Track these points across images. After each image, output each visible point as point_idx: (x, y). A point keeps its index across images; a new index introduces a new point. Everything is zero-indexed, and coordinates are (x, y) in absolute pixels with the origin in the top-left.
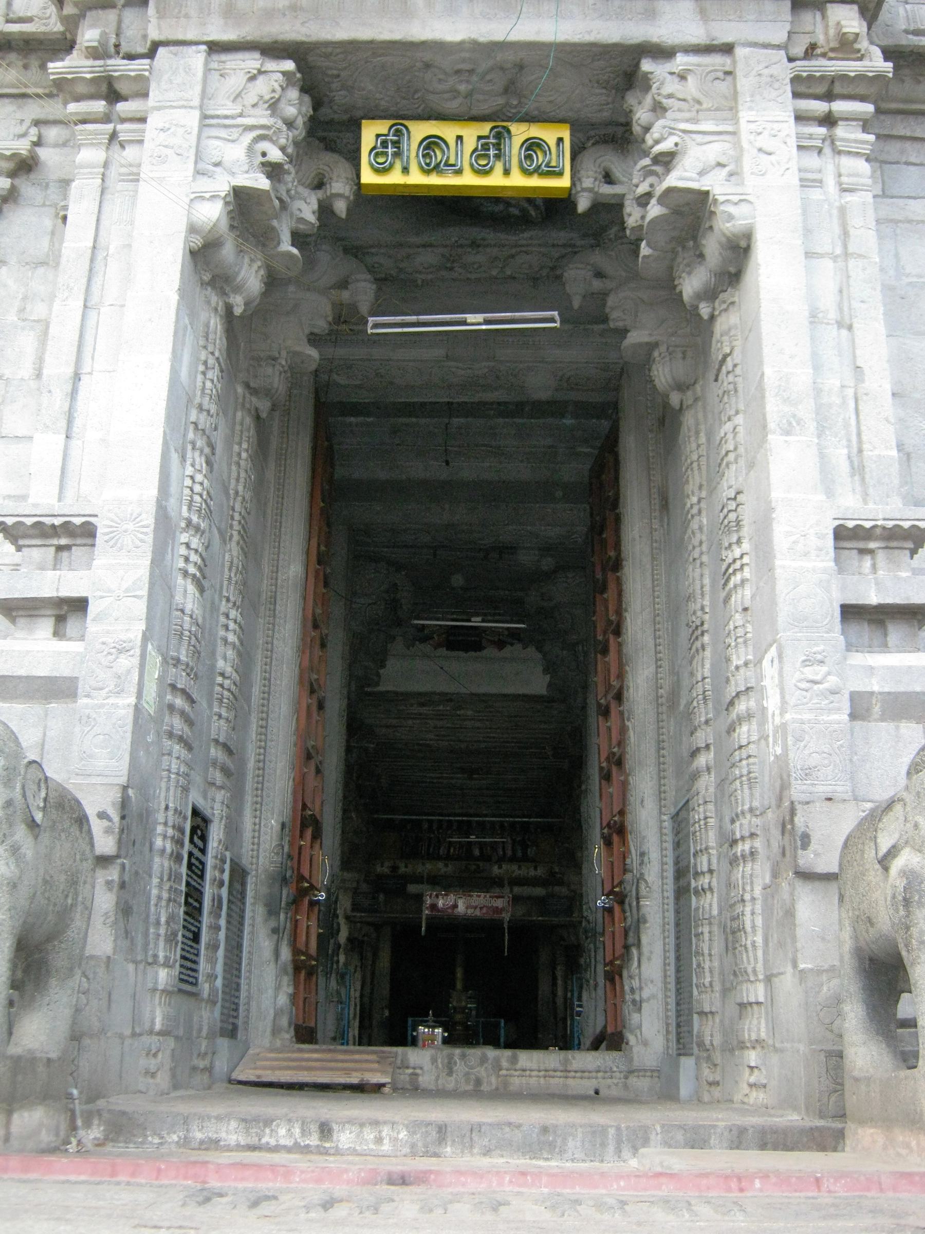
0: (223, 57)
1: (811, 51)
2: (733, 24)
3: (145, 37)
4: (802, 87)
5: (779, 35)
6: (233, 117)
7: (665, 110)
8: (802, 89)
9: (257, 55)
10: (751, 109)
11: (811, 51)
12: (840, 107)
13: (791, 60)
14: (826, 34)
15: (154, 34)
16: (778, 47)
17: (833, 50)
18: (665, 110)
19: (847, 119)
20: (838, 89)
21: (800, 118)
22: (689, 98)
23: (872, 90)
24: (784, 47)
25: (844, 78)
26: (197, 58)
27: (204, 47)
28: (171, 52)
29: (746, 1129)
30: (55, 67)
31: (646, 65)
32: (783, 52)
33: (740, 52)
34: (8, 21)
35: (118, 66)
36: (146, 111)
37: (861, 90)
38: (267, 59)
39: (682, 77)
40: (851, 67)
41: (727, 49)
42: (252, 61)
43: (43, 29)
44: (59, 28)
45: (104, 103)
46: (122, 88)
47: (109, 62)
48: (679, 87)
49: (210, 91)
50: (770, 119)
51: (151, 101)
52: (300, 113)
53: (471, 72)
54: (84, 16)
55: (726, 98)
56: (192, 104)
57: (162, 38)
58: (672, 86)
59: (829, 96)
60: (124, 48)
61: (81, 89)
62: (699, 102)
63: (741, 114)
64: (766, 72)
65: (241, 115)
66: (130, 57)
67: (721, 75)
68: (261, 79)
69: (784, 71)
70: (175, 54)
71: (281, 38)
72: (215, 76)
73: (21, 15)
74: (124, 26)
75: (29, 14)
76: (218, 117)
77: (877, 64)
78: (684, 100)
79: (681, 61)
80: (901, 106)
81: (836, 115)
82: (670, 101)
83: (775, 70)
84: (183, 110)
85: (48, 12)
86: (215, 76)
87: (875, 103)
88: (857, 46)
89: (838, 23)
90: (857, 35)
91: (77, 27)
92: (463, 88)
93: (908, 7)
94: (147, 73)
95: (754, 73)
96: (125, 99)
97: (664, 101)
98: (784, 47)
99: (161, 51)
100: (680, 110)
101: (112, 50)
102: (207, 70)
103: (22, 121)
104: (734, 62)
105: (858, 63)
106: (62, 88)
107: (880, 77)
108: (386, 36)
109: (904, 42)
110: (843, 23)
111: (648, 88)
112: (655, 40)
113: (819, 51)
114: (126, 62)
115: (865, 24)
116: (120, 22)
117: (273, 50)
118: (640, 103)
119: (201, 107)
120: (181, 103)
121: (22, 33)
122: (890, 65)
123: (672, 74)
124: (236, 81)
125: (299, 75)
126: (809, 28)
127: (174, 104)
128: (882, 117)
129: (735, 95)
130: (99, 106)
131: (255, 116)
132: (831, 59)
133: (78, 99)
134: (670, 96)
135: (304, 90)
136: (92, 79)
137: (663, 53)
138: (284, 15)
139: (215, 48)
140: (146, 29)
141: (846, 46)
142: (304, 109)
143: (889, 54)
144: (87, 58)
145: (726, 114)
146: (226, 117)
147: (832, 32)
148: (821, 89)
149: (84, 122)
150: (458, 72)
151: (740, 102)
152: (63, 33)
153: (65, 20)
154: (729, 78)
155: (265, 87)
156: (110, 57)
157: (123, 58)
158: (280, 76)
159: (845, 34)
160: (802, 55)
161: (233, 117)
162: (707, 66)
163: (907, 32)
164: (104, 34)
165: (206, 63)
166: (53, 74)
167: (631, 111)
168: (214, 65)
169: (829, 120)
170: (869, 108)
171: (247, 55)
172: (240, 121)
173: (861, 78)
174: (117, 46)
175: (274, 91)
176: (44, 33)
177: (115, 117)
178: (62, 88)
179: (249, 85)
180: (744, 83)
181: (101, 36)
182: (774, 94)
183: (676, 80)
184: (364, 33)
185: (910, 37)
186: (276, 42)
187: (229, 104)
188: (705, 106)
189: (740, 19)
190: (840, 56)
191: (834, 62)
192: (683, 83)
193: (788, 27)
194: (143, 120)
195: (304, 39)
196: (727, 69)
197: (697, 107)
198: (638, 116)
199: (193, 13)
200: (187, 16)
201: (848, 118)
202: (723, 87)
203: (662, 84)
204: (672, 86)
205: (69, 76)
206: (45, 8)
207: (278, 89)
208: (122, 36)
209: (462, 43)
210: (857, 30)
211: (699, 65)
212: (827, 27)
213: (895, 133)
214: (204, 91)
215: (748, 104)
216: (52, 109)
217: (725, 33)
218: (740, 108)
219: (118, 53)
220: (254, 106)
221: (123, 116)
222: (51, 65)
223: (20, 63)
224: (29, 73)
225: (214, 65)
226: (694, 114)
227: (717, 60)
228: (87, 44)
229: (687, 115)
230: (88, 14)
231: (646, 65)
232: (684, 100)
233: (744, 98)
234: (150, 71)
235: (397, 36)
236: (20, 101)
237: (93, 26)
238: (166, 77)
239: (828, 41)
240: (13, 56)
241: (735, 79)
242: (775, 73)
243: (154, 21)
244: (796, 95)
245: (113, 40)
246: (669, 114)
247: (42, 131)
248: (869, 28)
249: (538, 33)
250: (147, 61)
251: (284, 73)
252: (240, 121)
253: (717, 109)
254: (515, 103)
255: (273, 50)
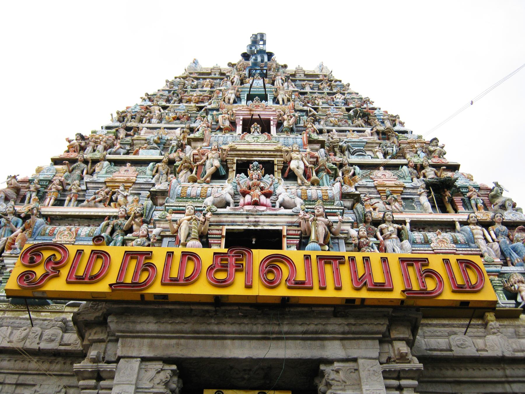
0: (147, 363)
1: (389, 360)
2: (356, 350)
3: (116, 354)
4: (387, 375)
5: (376, 354)
6: (149, 389)
7: (331, 385)
8: (387, 375)
9: (161, 363)
10: (367, 384)
11: (389, 360)
12: (404, 382)
13: (381, 363)
14: (394, 352)
15: (119, 354)
16: (375, 359)
17: (397, 359)
18: (331, 385)
19: (407, 387)
20: (402, 375)
21: (388, 388)
22: (341, 380)
23: (416, 375)
24: (378, 359)
25: (404, 371)
26: (136, 364)
27: (139, 359)
28: (126, 361)
29: (21, 202)
30: (76, 366)
31: (322, 367)
32: (377, 361)
33: (360, 361)
34: (60, 345)
35: (103, 366)
36: (112, 385)
37: (411, 375)
38: (165, 365)
39: (337, 371)
40: (406, 366)
41: (355, 360)
42: (159, 365)
43: (74, 348)
44: (81, 348)
45: (95, 381)
46: (103, 375)
47: (100, 364)
48: (337, 376)
49: (140, 377)
50: (375, 388)
51: (115, 381)
52: (178, 386)
53: (250, 370)
54: (92, 345)
55: (356, 380)
56: (132, 383)
57: (123, 355)
58: (333, 375)
59: (399, 378)
60: (107, 359)
61: (86, 375)
62: (345, 382)
63: (363, 387)
64: (371, 369)
65: (152, 388)
66: (108, 362)
67: (353, 371)
68: (162, 372)
69: (379, 368)
70: (127, 362)
71: (172, 356)
72: (143, 371)
73: (66, 342)
74: (107, 350)
75: (69, 342)
76: (142, 388)
77: (416, 364)
78: (339, 381)
79: (336, 365)
80: (430, 379)
81: (403, 386)
82: (333, 382)
83: (375, 368)
84: (128, 385)
85: (78, 342)
86: (143, 371)
87: (418, 380)
88: (407, 357)
89: (399, 349)
90: (407, 353)
91: (88, 349)
92: (246, 376)
93: (425, 340)
94: (114, 370)
95: (367, 369)
96: (104, 380)
97: (330, 382)
98: (378, 359)
99: (122, 360)
100: (337, 385)
101: (101, 359)
102: (140, 368)
103: (59, 386)
104: (358, 365)
105: (409, 364)
106: (80, 375)
107: (418, 370)
108: (215, 356)
109: (426, 354)
110: (400, 348)
111: (323, 376)
112: (325, 357)
113: (392, 360)
114: (106, 364)
115: (409, 348)
116: (106, 348)
117: (167, 361)
118: (320, 382)
119: (136, 384)
120: (127, 382)
121: (65, 350)
122: (422, 365)
123: (332, 370)
124: (152, 373)
125: (178, 371)
126: (387, 350)
127: (125, 383)
128: (422, 384)
129: (360, 378)
130: (93, 382)
131: (158, 388)
132: (397, 363)
133: (84, 379)
134: (333, 380)
135: (179, 377)
136: (91, 371)
137: (329, 362)
138: (173, 347)
139: (144, 359)
140: (116, 351)
141: (403, 358)
142: (179, 385)
143: (421, 359)
144: (90, 362)
145: (357, 387)
146: (146, 388)
147: (396, 352)
148: (395, 375)
149: (86, 389)
150: (245, 370)
151: (362, 382)
152: (82, 351)
153: (83, 346)
154: (357, 372)
155: (162, 376)
156: (100, 362)
157: (105, 363)
158: (170, 372)
159: (402, 353)
160: (385, 361)
161: (149, 389)
162: (347, 367)
163: (426, 350)
164: (99, 353)
165: (140, 366)
166: (76, 368)
167: (317, 386)
168: (143, 367)
169: (400, 388)
170: (416, 382)
171: (157, 363)
172: (152, 390)
173: (411, 370)
174: (104, 358)
175: (167, 378)
176: (74, 350)
177: (99, 387)
178: (80, 375)
179: (157, 375)
180: (363, 374)
181: (98, 353)
182: (376, 378)
183: (335, 373)
184: (206, 355)
185: (428, 352)
186: (169, 358)
187: (148, 383)
188: (347, 383)
189: (359, 348)
190: (401, 361)
191: (399, 364)
192: (338, 374)
193: (379, 351)
194: (111, 389)
195: (181, 356)
196: (356, 368)
197: (344, 384)
198: (320, 388)
199: (136, 345)
200: (134, 347)
201: (408, 387)
202: (354, 375)
203: (329, 374)
204: (333, 375)
205: (82, 370)
206: (76, 340)
207: (169, 377)
208: (106, 354)
209: (246, 359)
210: (406, 351)
211: (344, 367)
212: (394, 350)
213: (428, 390)
214: (138, 378)
215: (366, 383)
216: (73, 381)
217: (354, 353)
218: (362, 384)
219: (103, 360)
220: (158, 384)
221: (102, 387)
222: (75, 365)
223: (63, 362)
224: (66, 366)
225: (143, 367)
226: (343, 387)
227: (351, 365)
228: (91, 357)
229: (340, 387)
230: (93, 344)
231: (322, 367)
232: (339, 381)
233: (364, 381)
234: (116, 368)
235: (219, 356)
236: (60, 377)
237: (95, 349)
238: (122, 371)
239: (395, 356)
240: (60, 359)
241: (359, 372)
242: (375, 370)
243: (120, 348)
244: (385, 378)
245: (102, 356)
246: (333, 387)
247: (67, 390)
248: (411, 349)
249: (277, 354)
250: (115, 364)
251: (172, 370)
252: (152, 390)
253: (353, 385)
254: (268, 382)
255: (167, 361)
